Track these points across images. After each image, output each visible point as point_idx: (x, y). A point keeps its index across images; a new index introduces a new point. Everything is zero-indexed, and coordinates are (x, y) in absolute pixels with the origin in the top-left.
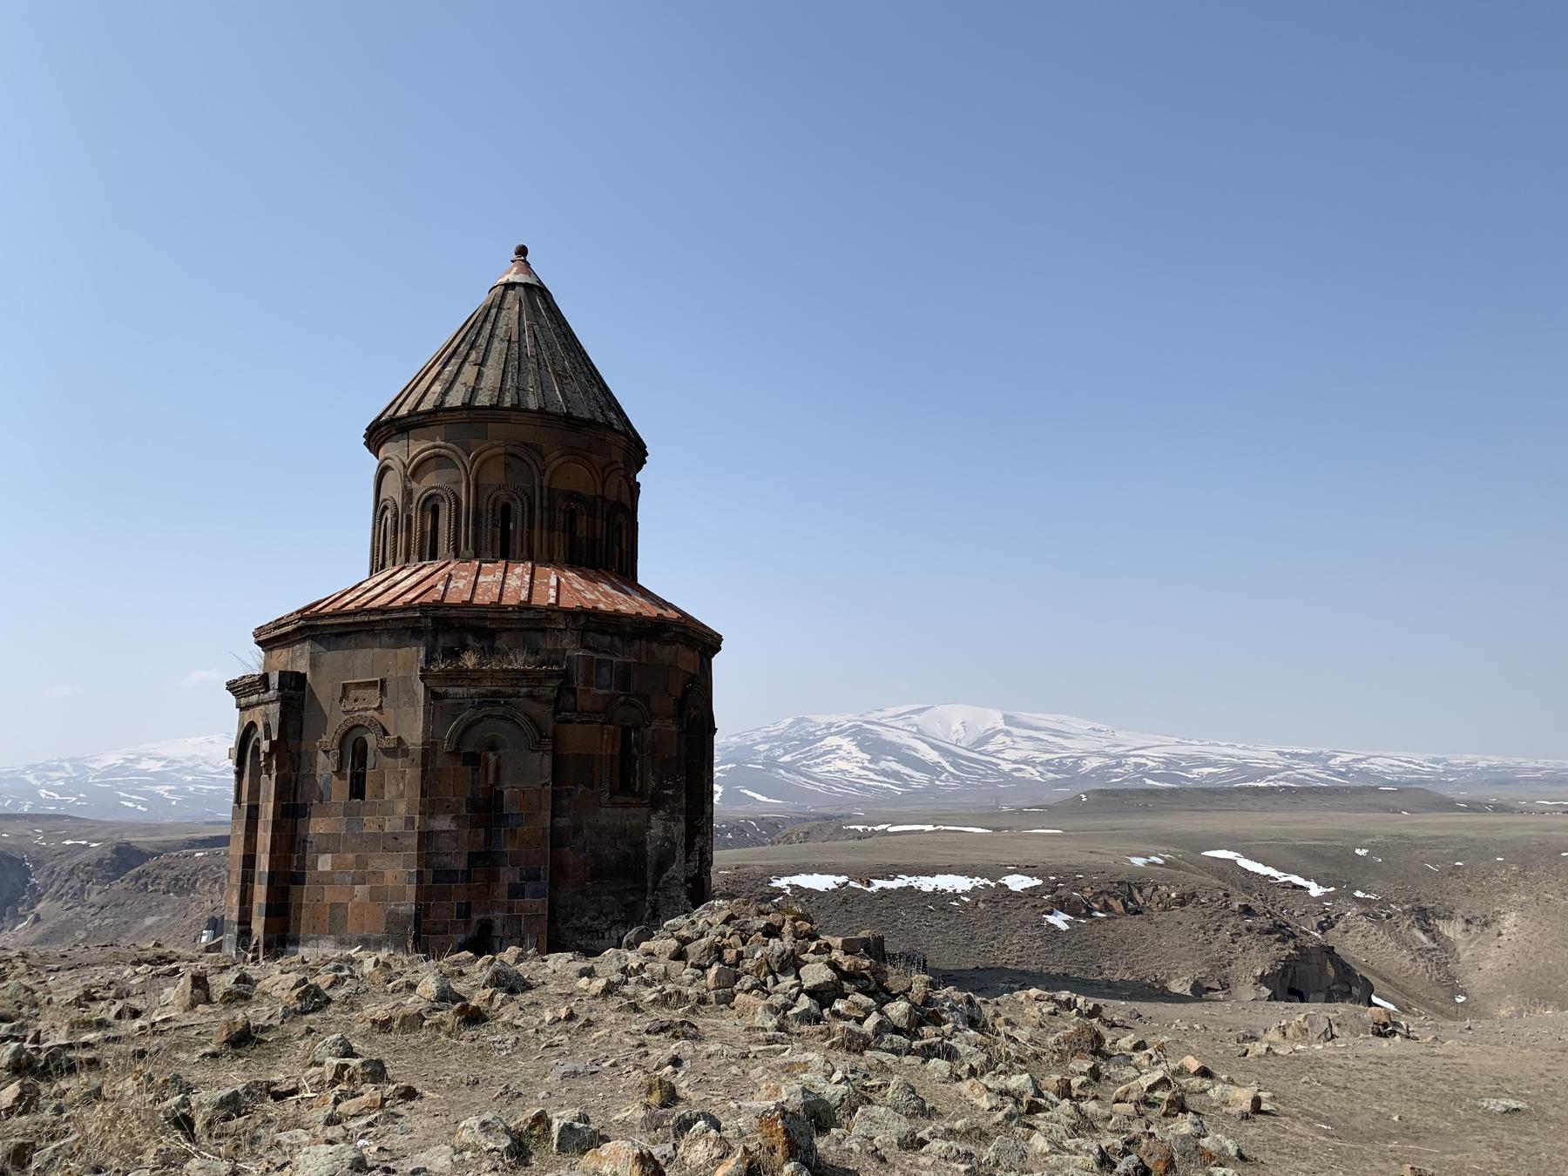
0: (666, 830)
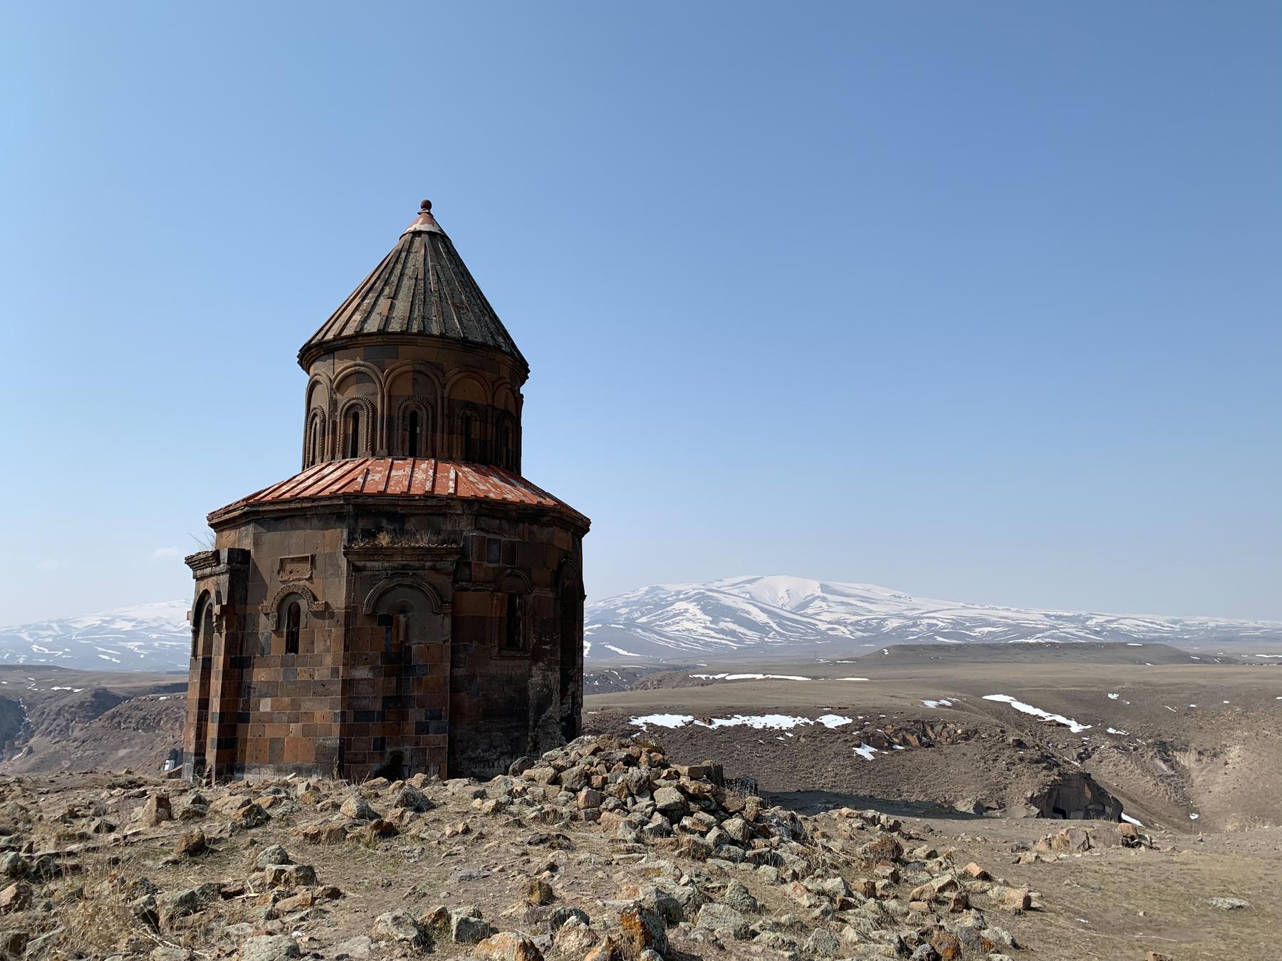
0: (544, 678)
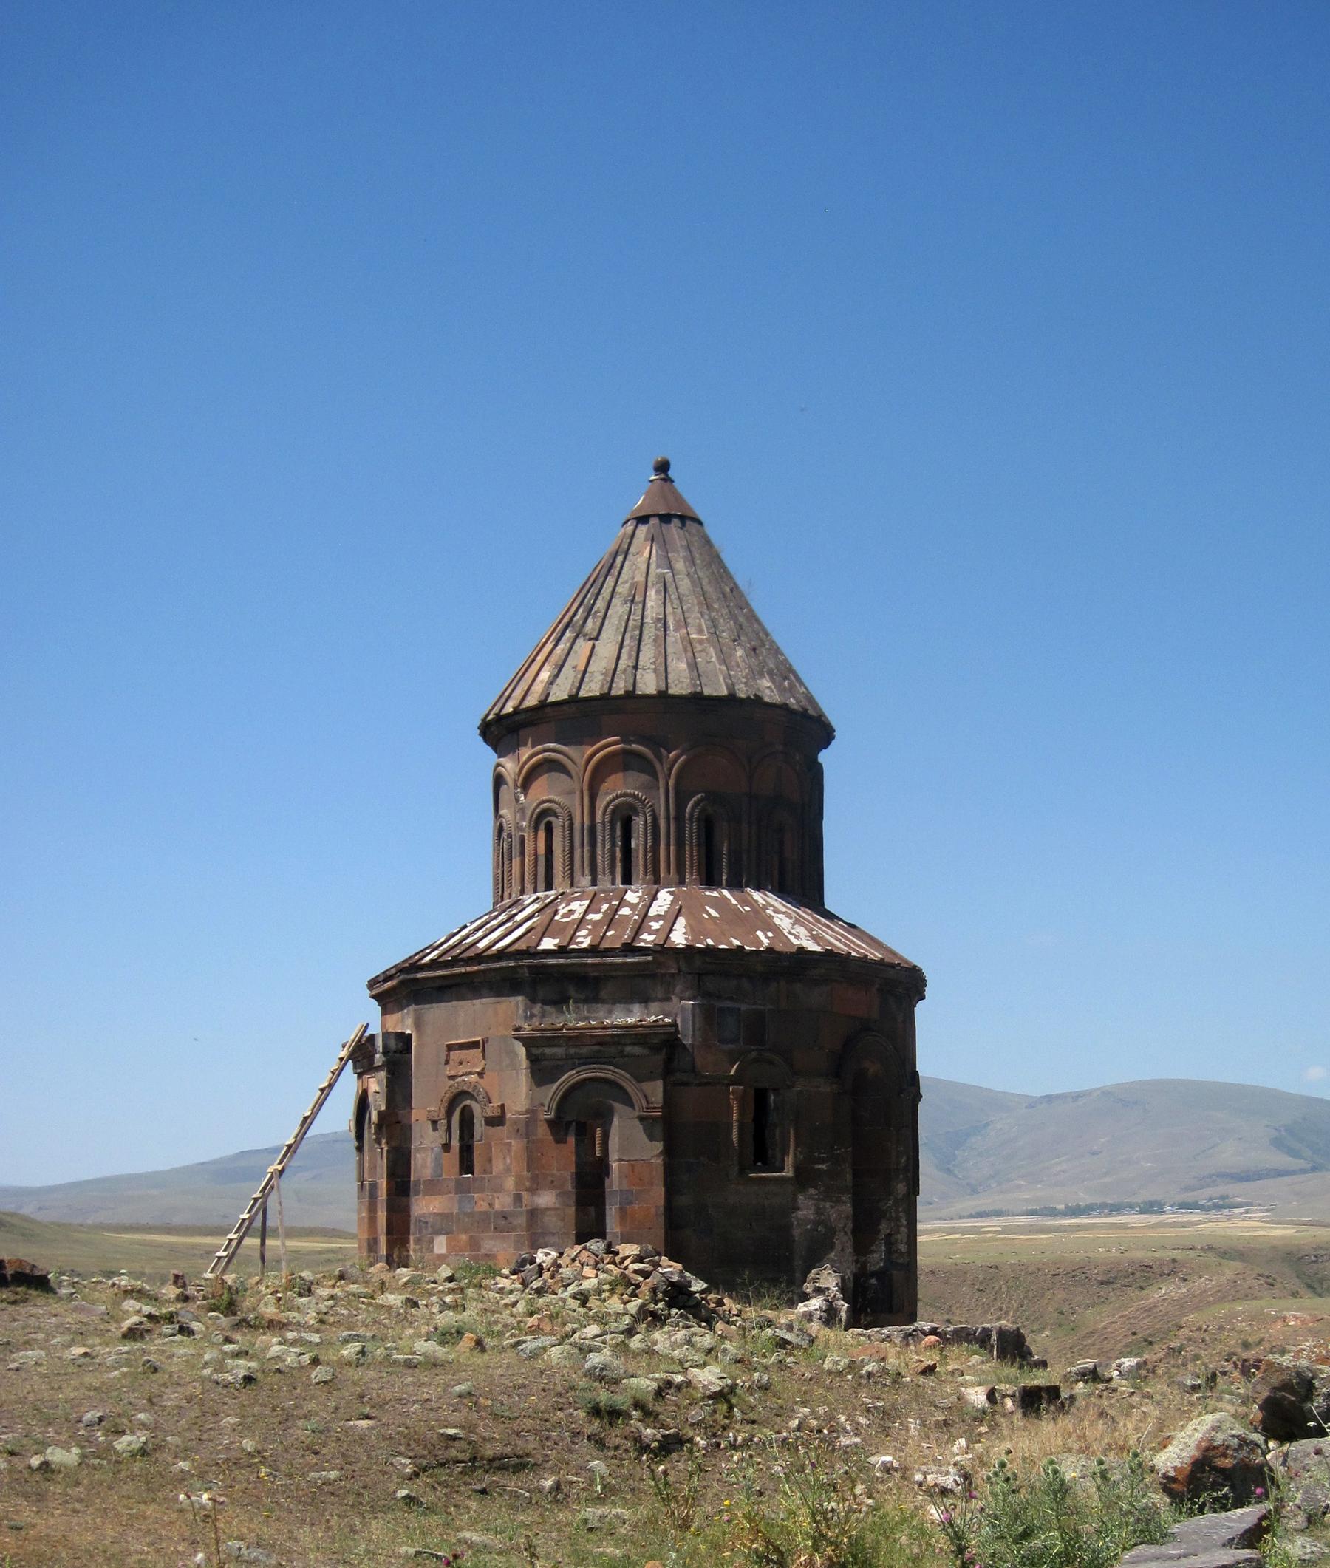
0: (819, 1211)
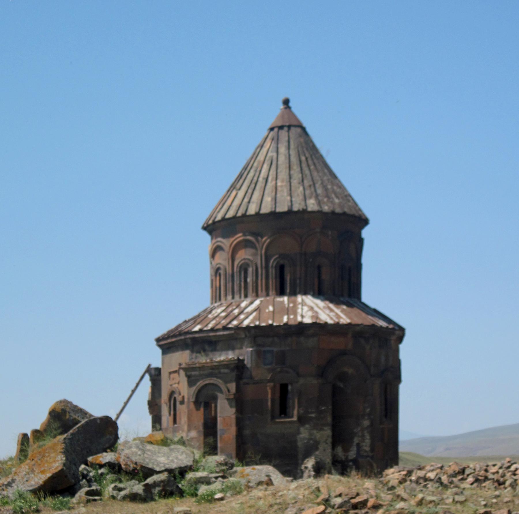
0: (311, 434)
